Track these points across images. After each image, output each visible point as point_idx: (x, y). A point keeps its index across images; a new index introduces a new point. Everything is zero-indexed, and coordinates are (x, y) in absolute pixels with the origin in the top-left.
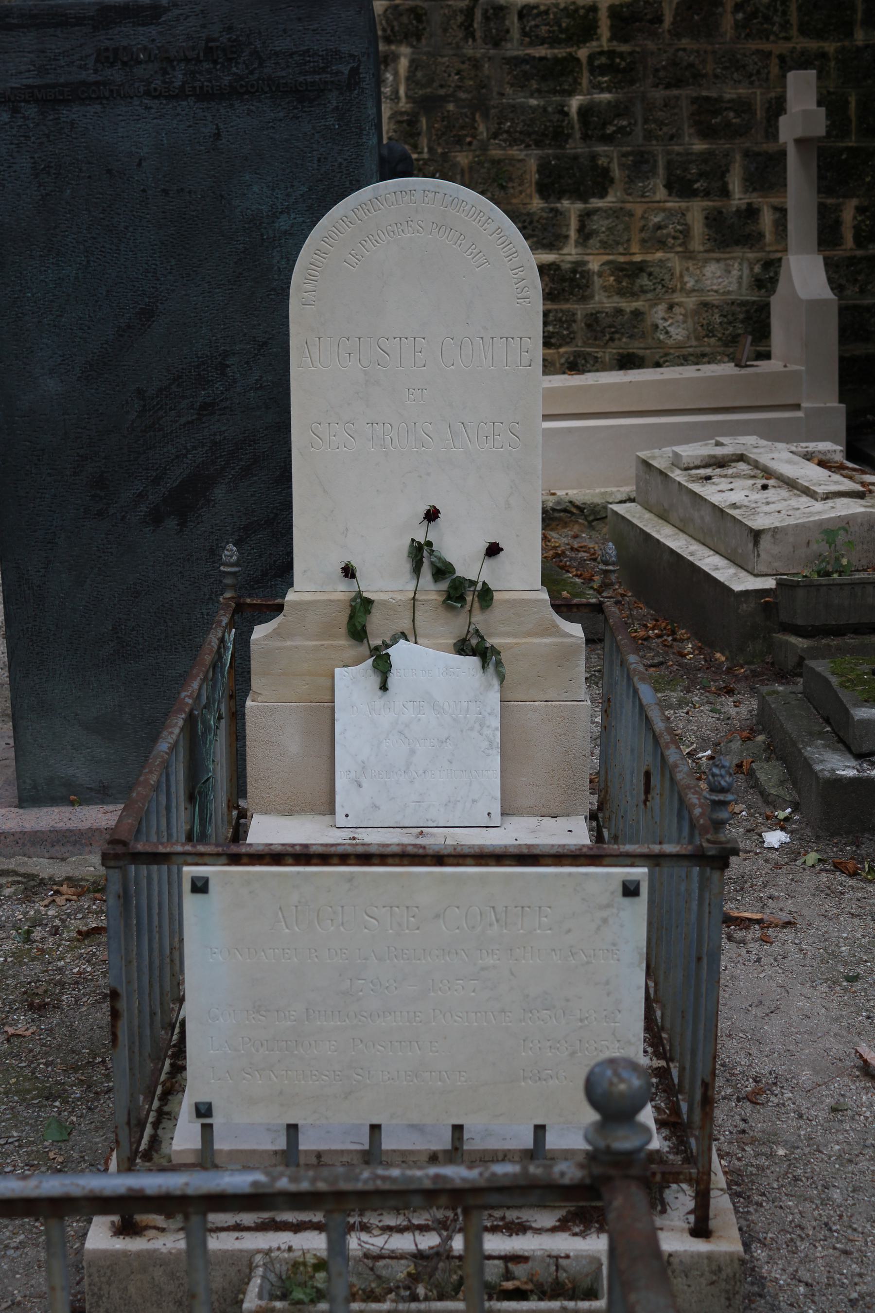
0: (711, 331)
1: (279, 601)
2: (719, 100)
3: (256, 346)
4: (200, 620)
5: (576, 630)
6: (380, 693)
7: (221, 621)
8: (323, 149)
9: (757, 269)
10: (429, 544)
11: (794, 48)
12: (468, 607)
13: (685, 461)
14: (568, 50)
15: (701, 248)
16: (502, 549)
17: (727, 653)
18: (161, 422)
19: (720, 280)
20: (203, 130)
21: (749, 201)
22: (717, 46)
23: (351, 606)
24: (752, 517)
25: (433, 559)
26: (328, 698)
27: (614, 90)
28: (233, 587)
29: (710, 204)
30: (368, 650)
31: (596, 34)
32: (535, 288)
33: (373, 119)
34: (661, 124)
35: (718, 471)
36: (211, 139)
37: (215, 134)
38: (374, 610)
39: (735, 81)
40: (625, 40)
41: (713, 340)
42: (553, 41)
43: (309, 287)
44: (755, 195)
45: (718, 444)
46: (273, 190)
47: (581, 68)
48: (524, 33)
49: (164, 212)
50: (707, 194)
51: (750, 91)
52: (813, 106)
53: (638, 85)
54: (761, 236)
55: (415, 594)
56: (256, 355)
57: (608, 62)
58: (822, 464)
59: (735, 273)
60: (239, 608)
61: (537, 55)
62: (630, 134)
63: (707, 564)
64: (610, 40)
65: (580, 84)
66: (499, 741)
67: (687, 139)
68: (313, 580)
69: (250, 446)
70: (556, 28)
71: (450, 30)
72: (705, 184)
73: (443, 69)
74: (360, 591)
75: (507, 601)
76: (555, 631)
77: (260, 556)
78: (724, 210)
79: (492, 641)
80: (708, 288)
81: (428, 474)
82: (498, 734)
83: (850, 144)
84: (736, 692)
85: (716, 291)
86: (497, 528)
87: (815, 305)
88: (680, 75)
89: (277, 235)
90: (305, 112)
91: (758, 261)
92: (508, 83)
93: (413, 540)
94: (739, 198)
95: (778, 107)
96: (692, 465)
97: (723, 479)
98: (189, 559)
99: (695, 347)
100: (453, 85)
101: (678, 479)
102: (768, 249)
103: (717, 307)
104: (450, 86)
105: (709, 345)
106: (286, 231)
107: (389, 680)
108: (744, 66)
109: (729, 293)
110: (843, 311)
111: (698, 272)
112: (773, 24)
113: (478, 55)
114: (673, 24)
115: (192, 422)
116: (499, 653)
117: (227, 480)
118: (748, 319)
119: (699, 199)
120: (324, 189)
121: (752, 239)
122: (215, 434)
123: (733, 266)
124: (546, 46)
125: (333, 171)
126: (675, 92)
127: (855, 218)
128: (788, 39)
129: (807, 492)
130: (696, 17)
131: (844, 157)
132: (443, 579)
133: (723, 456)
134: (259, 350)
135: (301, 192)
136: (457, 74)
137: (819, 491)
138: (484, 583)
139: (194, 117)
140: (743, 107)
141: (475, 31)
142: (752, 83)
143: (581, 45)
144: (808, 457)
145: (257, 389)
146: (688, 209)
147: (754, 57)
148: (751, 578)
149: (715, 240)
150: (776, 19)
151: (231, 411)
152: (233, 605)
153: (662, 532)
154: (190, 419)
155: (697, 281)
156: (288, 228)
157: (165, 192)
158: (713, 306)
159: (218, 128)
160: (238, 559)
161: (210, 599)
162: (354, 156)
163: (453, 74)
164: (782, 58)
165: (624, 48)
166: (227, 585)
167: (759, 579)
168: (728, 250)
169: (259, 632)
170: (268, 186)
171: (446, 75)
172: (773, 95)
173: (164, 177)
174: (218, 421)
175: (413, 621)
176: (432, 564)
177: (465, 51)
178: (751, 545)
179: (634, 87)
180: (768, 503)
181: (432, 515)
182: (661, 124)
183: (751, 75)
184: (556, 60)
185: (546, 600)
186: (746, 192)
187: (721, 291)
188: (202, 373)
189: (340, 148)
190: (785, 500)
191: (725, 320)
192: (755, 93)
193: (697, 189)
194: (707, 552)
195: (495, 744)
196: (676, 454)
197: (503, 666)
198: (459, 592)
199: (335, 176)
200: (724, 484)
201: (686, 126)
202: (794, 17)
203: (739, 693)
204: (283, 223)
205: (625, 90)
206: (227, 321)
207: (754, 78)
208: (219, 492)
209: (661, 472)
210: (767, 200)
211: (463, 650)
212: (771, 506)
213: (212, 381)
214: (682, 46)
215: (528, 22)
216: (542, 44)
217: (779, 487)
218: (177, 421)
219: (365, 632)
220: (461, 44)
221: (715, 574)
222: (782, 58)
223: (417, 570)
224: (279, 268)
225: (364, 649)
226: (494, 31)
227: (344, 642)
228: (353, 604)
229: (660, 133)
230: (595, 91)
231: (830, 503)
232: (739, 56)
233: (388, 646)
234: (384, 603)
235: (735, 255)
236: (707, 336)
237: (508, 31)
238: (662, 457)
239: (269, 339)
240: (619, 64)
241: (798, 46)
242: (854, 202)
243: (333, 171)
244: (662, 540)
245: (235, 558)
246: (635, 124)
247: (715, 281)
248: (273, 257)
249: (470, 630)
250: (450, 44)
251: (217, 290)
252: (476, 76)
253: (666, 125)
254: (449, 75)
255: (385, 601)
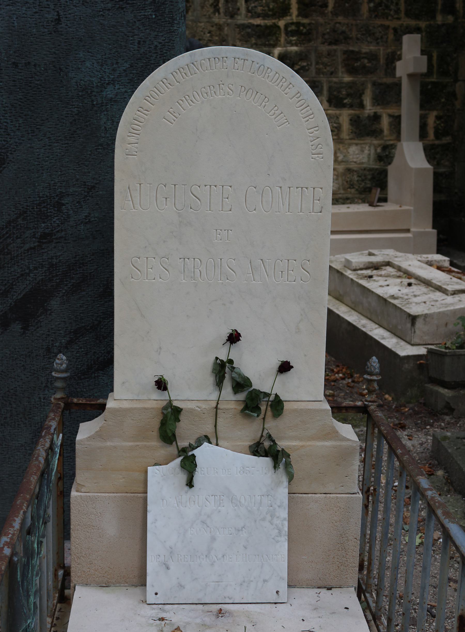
0: (352, 185)
1: (101, 401)
2: (359, 52)
3: (86, 189)
4: (38, 403)
5: (347, 431)
6: (187, 488)
7: (51, 426)
8: (142, 34)
9: (379, 150)
10: (231, 362)
11: (402, 24)
12: (262, 416)
13: (354, 265)
14: (273, 21)
15: (347, 137)
16: (292, 367)
17: (393, 395)
18: (9, 248)
19: (358, 156)
20: (47, 15)
21: (375, 111)
22: (358, 21)
23: (163, 413)
24: (408, 306)
25: (234, 375)
26: (141, 489)
27: (299, 45)
28: (63, 389)
29: (353, 112)
30: (176, 450)
31: (289, 12)
32: (328, 145)
33: (183, 11)
34: (325, 65)
35: (375, 272)
36: (53, 24)
37: (56, 19)
38: (182, 417)
39: (368, 42)
40: (306, 16)
41: (353, 191)
42: (265, 16)
43: (132, 140)
44: (379, 107)
45: (370, 254)
46: (102, 65)
47: (280, 32)
48: (248, 11)
49: (14, 81)
50: (351, 106)
51: (377, 48)
52: (418, 54)
53: (313, 42)
54: (382, 131)
55: (218, 403)
56: (86, 196)
57: (296, 29)
58: (439, 268)
59: (366, 152)
60: (68, 406)
61: (255, 23)
62: (308, 70)
63: (376, 335)
64: (298, 16)
65: (280, 41)
66: (286, 529)
67: (340, 74)
68: (129, 387)
69: (80, 267)
70: (266, 8)
71: (205, 8)
72: (350, 101)
73: (201, 29)
74: (170, 401)
75: (295, 410)
76: (334, 434)
77: (86, 354)
78: (361, 116)
79: (282, 444)
80: (351, 160)
81: (231, 303)
82: (286, 523)
83: (433, 80)
84: (407, 427)
85: (355, 162)
86: (289, 349)
87: (420, 171)
88: (336, 38)
89: (104, 102)
90: (128, 4)
91: (379, 145)
92: (238, 39)
93: (217, 358)
94: (369, 108)
95: (394, 58)
96: (358, 268)
97: (380, 278)
98: (30, 356)
99: (343, 194)
100: (206, 39)
101: (351, 276)
102: (385, 138)
103: (356, 171)
104: (204, 40)
105: (351, 193)
106: (112, 98)
107: (194, 479)
108: (374, 34)
109: (362, 163)
110: (436, 175)
111: (345, 151)
112: (391, 10)
113: (221, 22)
114: (333, 8)
115: (34, 248)
116: (288, 456)
117: (61, 294)
118: (373, 178)
119: (346, 109)
120: (142, 66)
121: (376, 133)
122: (52, 258)
123: (365, 148)
124: (261, 18)
125: (150, 52)
126: (334, 47)
127: (435, 122)
128: (399, 19)
129: (439, 289)
130: (347, 5)
131: (429, 87)
132: (242, 391)
133: (377, 263)
134: (88, 193)
135: (125, 68)
136: (209, 33)
137: (449, 289)
138: (276, 395)
139: (39, 5)
140: (373, 57)
141: (219, 8)
142: (378, 43)
143: (281, 19)
144: (430, 263)
145: (86, 223)
146: (340, 115)
147: (379, 28)
148: (409, 346)
149: (355, 133)
150: (392, 7)
151: (65, 240)
152: (62, 405)
153: (340, 309)
154: (32, 245)
155: (344, 156)
156: (113, 97)
157: (15, 65)
158: (353, 170)
159: (58, 15)
160: (67, 366)
161: (46, 386)
162: (166, 41)
163: (206, 33)
164: (395, 30)
165: (305, 21)
166: (57, 388)
167: (415, 348)
168: (363, 138)
169: (85, 431)
170: (98, 63)
171: (202, 33)
172: (389, 50)
173: (15, 52)
174: (55, 247)
175: (215, 426)
176: (233, 379)
177: (213, 20)
178: (409, 325)
179: (311, 44)
180: (415, 296)
181: (234, 338)
182: (325, 65)
183: (378, 39)
184: (266, 27)
185: (328, 410)
186: (373, 105)
187: (358, 162)
188: (42, 209)
189: (156, 33)
190: (426, 294)
191: (360, 179)
192: (379, 49)
193: (346, 103)
194: (374, 326)
195: (284, 532)
196: (348, 261)
197: (292, 467)
198: (254, 403)
199: (151, 56)
200: (382, 281)
201: (340, 67)
202: (402, 7)
203: (409, 428)
204: (109, 92)
205: (306, 45)
206: (63, 169)
207: (379, 41)
208: (55, 304)
209: (338, 271)
210: (386, 110)
211: (257, 451)
212: (418, 298)
213: (51, 216)
214: (338, 21)
215: (251, 4)
216: (258, 17)
217: (419, 284)
218: (22, 247)
219: (174, 435)
220: (212, 15)
221: (383, 342)
222: (395, 30)
223: (219, 383)
224: (105, 128)
225: (172, 449)
226: (231, 9)
227: (155, 443)
228: (165, 412)
229: (325, 70)
230: (288, 45)
231: (457, 298)
232: (371, 28)
233: (193, 448)
234: (191, 411)
235: (367, 141)
236: (350, 188)
237: (239, 9)
238: (336, 261)
239: (96, 184)
240: (303, 30)
241: (405, 23)
242: (435, 113)
243: (150, 52)
244: (342, 315)
245: (64, 366)
246: (311, 65)
247: (355, 156)
248: (100, 119)
249: (264, 434)
250: (205, 15)
251: (56, 144)
252: (220, 34)
253: (329, 66)
254: (204, 34)
255: (192, 409)
